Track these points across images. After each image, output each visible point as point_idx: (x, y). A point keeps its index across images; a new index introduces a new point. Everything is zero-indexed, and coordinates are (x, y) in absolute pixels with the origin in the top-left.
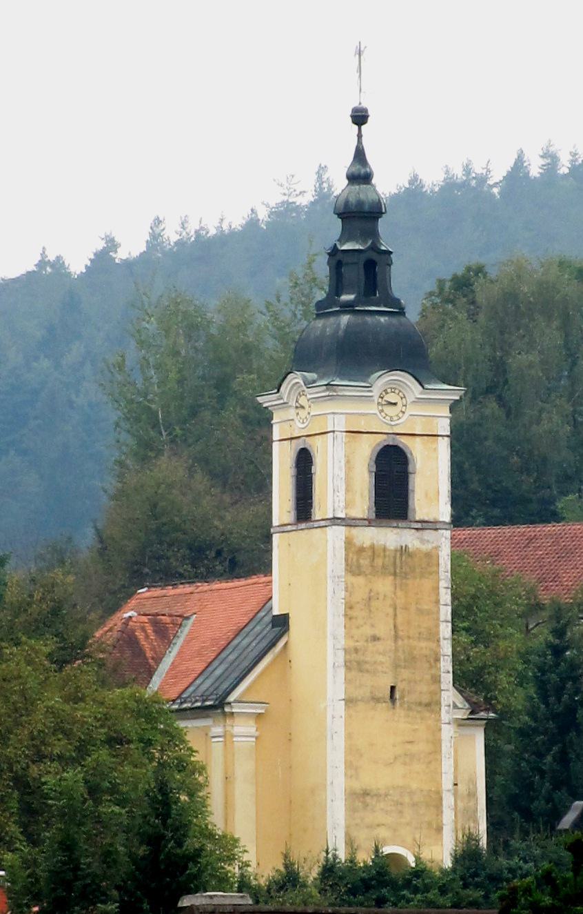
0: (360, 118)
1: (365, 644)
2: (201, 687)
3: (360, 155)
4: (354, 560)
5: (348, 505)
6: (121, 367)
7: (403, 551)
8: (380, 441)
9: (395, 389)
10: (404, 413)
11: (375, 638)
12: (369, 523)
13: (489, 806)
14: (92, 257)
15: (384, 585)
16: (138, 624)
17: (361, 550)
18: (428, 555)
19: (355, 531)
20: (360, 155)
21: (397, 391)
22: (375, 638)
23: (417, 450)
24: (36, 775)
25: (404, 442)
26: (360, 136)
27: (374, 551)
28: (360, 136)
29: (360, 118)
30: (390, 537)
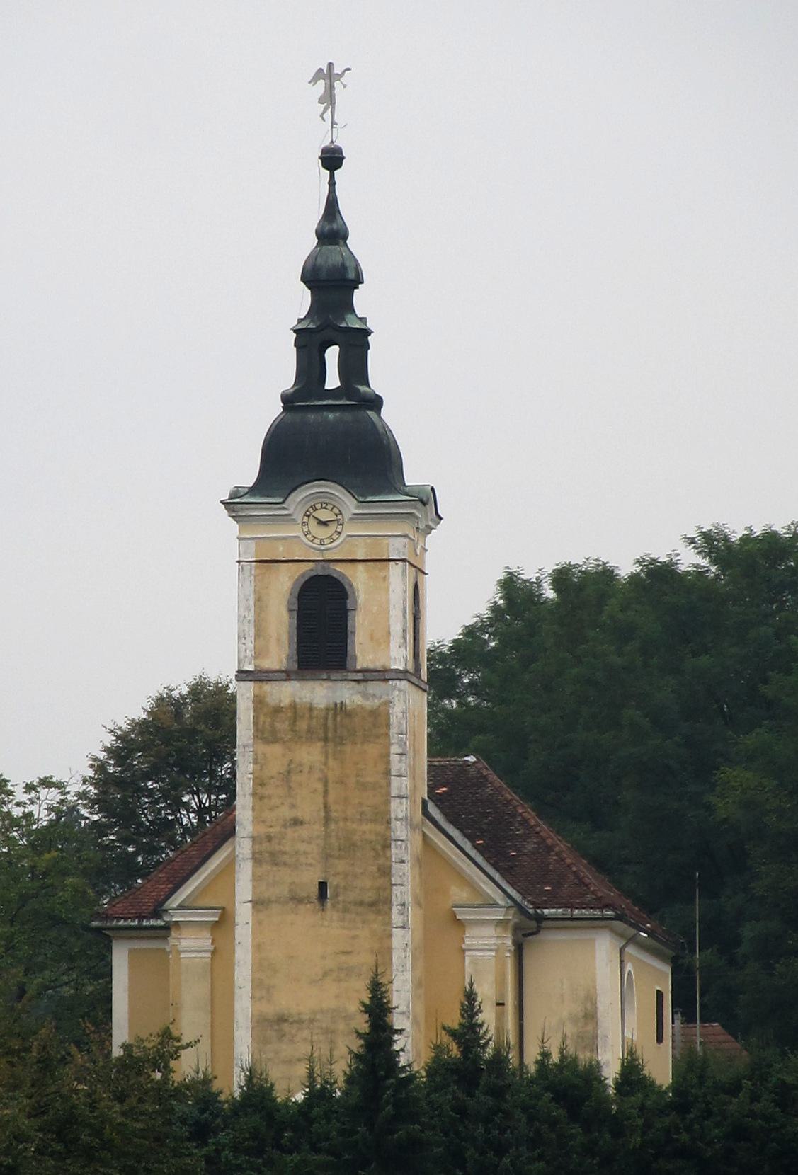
0: (332, 159)
3: (332, 208)
5: (257, 656)
7: (339, 709)
9: (327, 504)
10: (339, 533)
11: (297, 822)
15: (311, 754)
17: (278, 710)
18: (374, 713)
19: (267, 687)
20: (332, 208)
21: (330, 507)
23: (359, 580)
26: (332, 183)
28: (332, 183)
29: (332, 159)
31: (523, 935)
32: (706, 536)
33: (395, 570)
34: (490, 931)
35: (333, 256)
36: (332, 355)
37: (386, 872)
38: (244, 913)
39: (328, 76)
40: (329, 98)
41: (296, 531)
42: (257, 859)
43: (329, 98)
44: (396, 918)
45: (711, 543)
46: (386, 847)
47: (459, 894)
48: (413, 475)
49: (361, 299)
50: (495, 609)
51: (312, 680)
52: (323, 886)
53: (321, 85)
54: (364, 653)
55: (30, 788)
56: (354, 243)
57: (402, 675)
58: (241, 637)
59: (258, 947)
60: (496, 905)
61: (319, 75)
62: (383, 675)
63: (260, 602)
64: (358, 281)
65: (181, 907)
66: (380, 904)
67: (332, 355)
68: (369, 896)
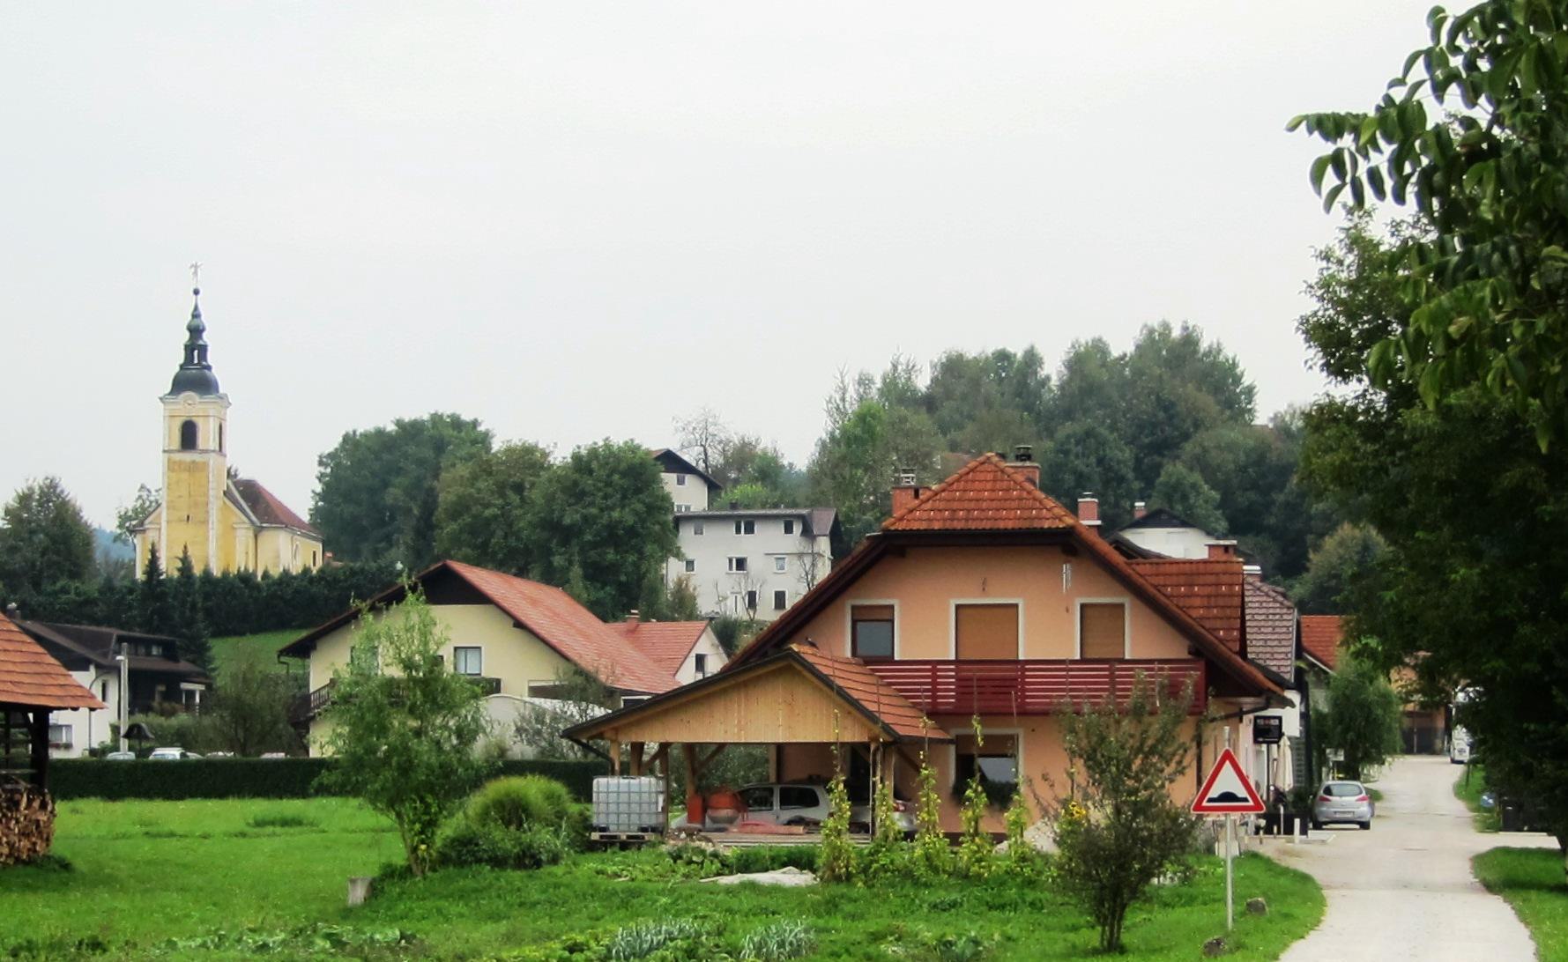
0: (196, 292)
1: (309, 586)
2: (1167, 565)
4: (703, 844)
5: (169, 445)
6: (1197, 425)
7: (194, 462)
8: (184, 419)
11: (180, 497)
12: (179, 451)
13: (758, 867)
14: (482, 428)
15: (185, 476)
16: (578, 624)
17: (175, 462)
18: (204, 463)
19: (172, 455)
22: (180, 497)
23: (200, 423)
24: (560, 952)
25: (194, 419)
27: (180, 463)
29: (196, 292)
30: (188, 457)
31: (783, 594)
32: (398, 421)
33: (211, 419)
34: (244, 531)
35: (196, 321)
36: (196, 352)
37: (207, 512)
38: (164, 524)
39: (196, 267)
40: (195, 273)
41: (180, 407)
42: (168, 508)
43: (195, 273)
44: (210, 526)
45: (399, 423)
46: (207, 504)
47: (234, 519)
48: (222, 390)
49: (205, 335)
50: (528, 459)
51: (1049, 544)
52: (188, 517)
53: (193, 270)
54: (201, 443)
55: (157, 491)
56: (203, 318)
57: (214, 451)
58: (164, 439)
59: (168, 535)
60: (244, 523)
61: (192, 266)
62: (206, 451)
63: (170, 428)
64: (203, 330)
65: (150, 523)
66: (205, 522)
67: (196, 352)
68: (202, 520)
